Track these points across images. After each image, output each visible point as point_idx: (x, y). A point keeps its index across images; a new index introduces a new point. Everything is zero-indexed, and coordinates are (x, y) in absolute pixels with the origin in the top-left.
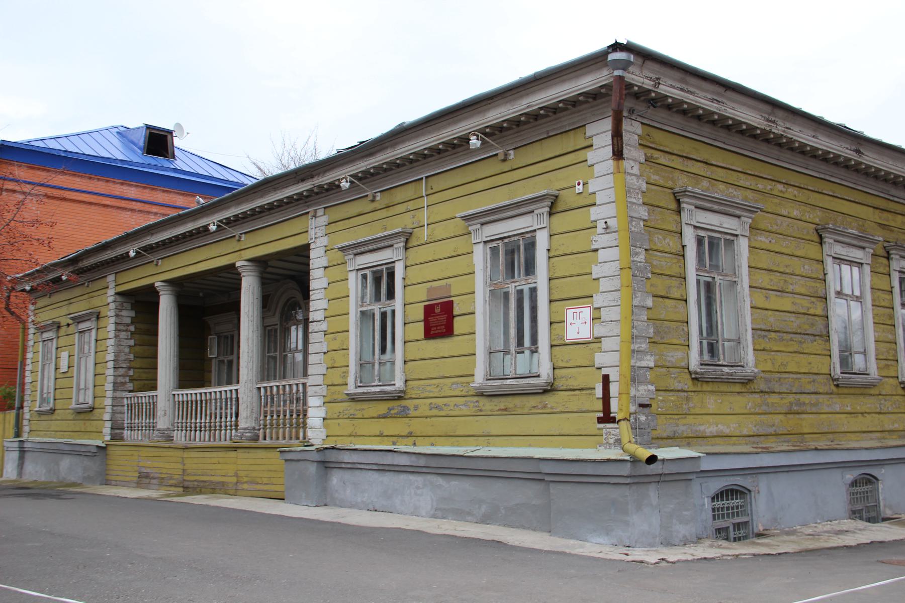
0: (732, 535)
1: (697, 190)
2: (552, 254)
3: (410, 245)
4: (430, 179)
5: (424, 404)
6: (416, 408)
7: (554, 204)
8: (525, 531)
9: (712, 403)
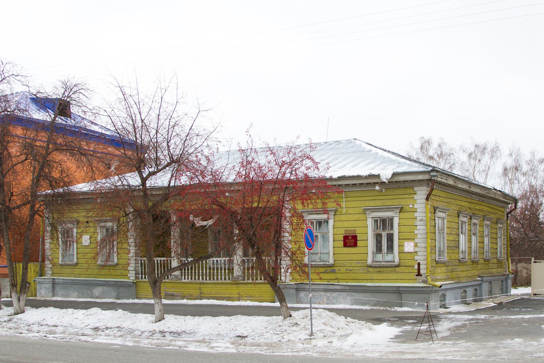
5: (343, 270)
7: (401, 210)
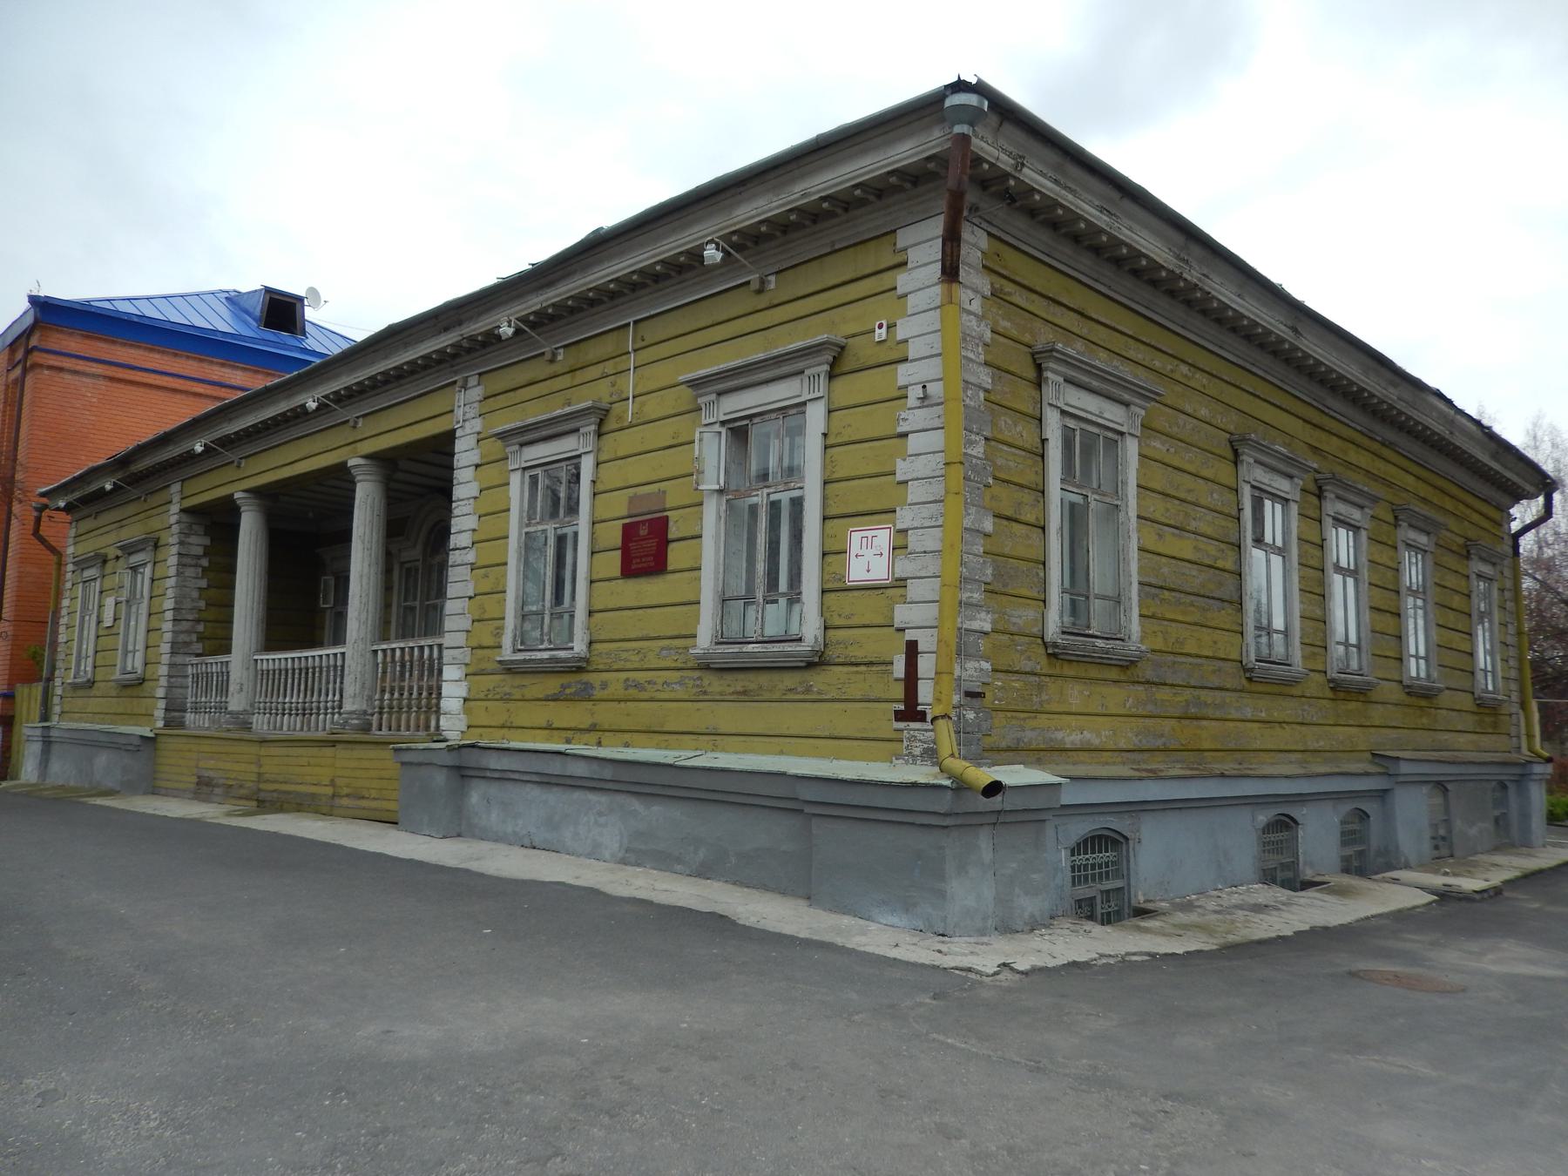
0: (1099, 911)
1: (1070, 351)
2: (831, 441)
3: (605, 429)
4: (641, 325)
6: (604, 685)
7: (837, 360)
8: (769, 895)
9: (1077, 696)
